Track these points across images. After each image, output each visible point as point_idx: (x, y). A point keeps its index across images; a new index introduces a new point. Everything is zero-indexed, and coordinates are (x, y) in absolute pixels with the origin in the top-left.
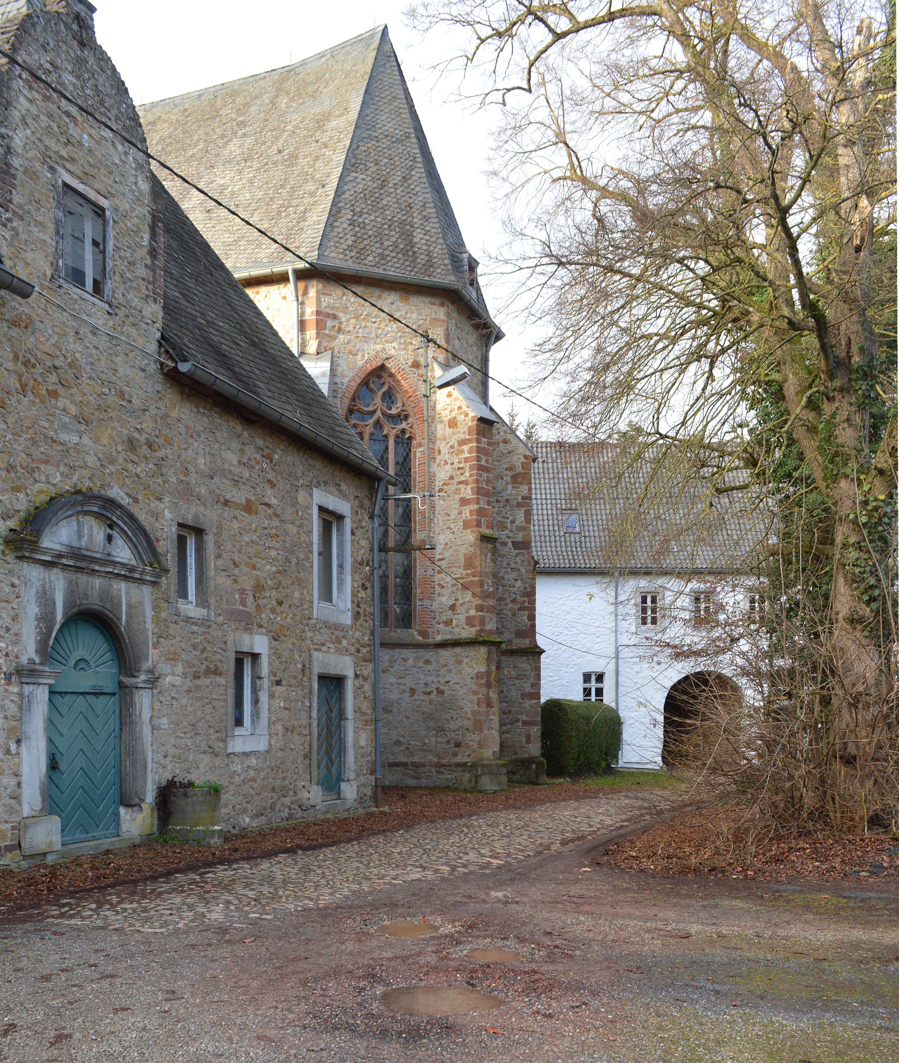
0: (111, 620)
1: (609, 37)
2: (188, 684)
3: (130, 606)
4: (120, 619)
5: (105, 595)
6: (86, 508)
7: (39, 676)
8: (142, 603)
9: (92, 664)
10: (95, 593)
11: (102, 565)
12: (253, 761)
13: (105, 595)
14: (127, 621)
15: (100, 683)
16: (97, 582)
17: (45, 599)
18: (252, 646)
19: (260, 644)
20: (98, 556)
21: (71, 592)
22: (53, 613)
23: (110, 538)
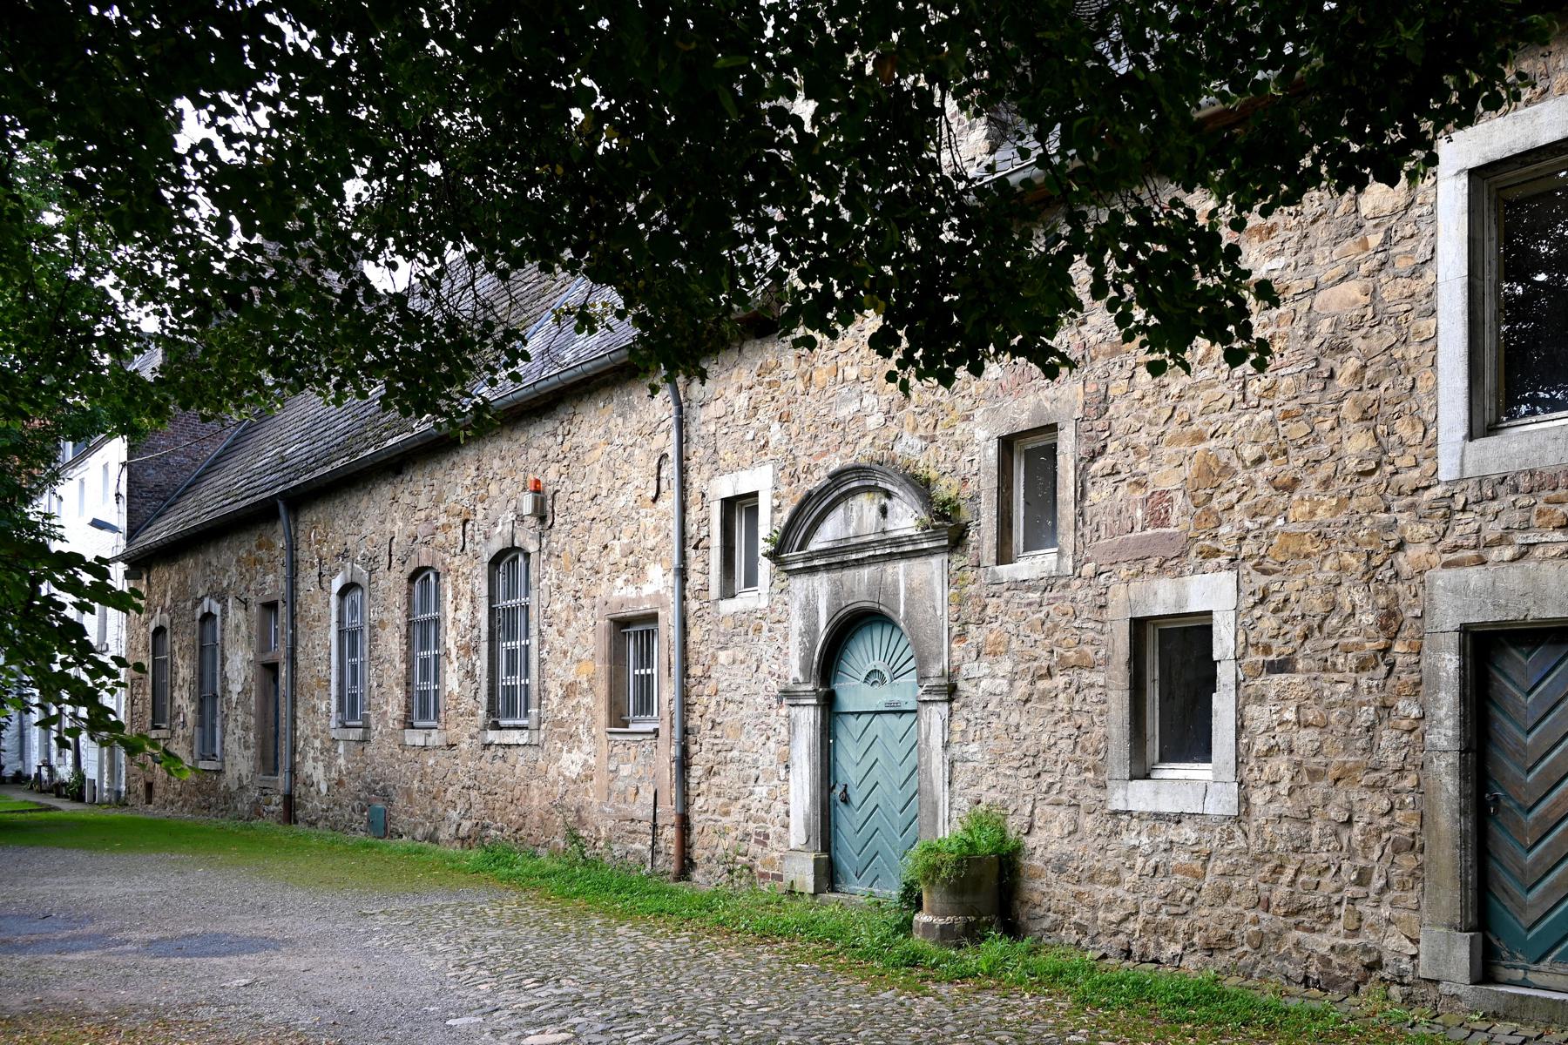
0: (850, 613)
1: (1531, 977)
2: (1022, 688)
3: (910, 591)
4: (897, 612)
5: (878, 586)
6: (844, 489)
7: (799, 697)
8: (929, 582)
9: (887, 675)
10: (863, 588)
11: (858, 551)
12: (1188, 832)
13: (878, 586)
14: (907, 612)
15: (897, 699)
16: (866, 573)
17: (810, 611)
18: (1181, 600)
19: (1210, 592)
20: (872, 538)
21: (835, 594)
22: (816, 624)
23: (884, 511)
